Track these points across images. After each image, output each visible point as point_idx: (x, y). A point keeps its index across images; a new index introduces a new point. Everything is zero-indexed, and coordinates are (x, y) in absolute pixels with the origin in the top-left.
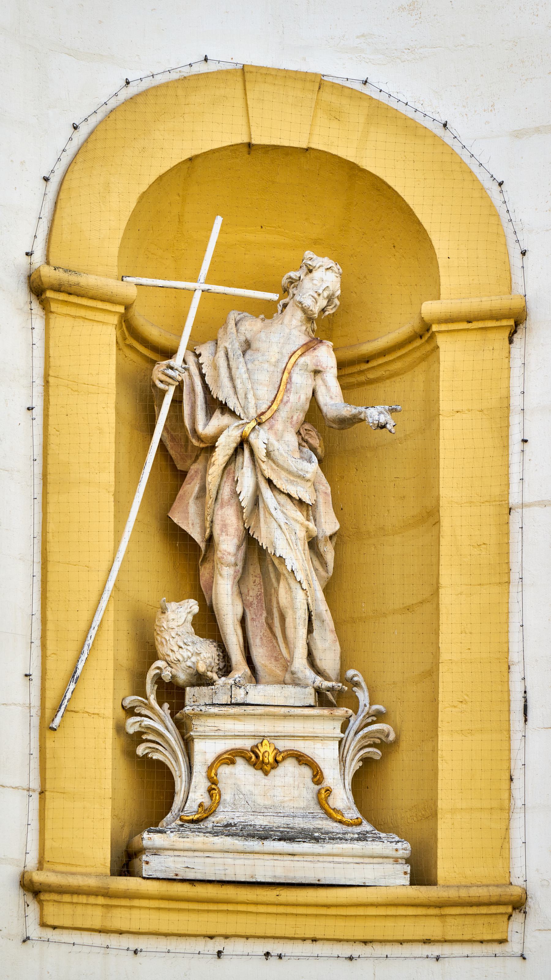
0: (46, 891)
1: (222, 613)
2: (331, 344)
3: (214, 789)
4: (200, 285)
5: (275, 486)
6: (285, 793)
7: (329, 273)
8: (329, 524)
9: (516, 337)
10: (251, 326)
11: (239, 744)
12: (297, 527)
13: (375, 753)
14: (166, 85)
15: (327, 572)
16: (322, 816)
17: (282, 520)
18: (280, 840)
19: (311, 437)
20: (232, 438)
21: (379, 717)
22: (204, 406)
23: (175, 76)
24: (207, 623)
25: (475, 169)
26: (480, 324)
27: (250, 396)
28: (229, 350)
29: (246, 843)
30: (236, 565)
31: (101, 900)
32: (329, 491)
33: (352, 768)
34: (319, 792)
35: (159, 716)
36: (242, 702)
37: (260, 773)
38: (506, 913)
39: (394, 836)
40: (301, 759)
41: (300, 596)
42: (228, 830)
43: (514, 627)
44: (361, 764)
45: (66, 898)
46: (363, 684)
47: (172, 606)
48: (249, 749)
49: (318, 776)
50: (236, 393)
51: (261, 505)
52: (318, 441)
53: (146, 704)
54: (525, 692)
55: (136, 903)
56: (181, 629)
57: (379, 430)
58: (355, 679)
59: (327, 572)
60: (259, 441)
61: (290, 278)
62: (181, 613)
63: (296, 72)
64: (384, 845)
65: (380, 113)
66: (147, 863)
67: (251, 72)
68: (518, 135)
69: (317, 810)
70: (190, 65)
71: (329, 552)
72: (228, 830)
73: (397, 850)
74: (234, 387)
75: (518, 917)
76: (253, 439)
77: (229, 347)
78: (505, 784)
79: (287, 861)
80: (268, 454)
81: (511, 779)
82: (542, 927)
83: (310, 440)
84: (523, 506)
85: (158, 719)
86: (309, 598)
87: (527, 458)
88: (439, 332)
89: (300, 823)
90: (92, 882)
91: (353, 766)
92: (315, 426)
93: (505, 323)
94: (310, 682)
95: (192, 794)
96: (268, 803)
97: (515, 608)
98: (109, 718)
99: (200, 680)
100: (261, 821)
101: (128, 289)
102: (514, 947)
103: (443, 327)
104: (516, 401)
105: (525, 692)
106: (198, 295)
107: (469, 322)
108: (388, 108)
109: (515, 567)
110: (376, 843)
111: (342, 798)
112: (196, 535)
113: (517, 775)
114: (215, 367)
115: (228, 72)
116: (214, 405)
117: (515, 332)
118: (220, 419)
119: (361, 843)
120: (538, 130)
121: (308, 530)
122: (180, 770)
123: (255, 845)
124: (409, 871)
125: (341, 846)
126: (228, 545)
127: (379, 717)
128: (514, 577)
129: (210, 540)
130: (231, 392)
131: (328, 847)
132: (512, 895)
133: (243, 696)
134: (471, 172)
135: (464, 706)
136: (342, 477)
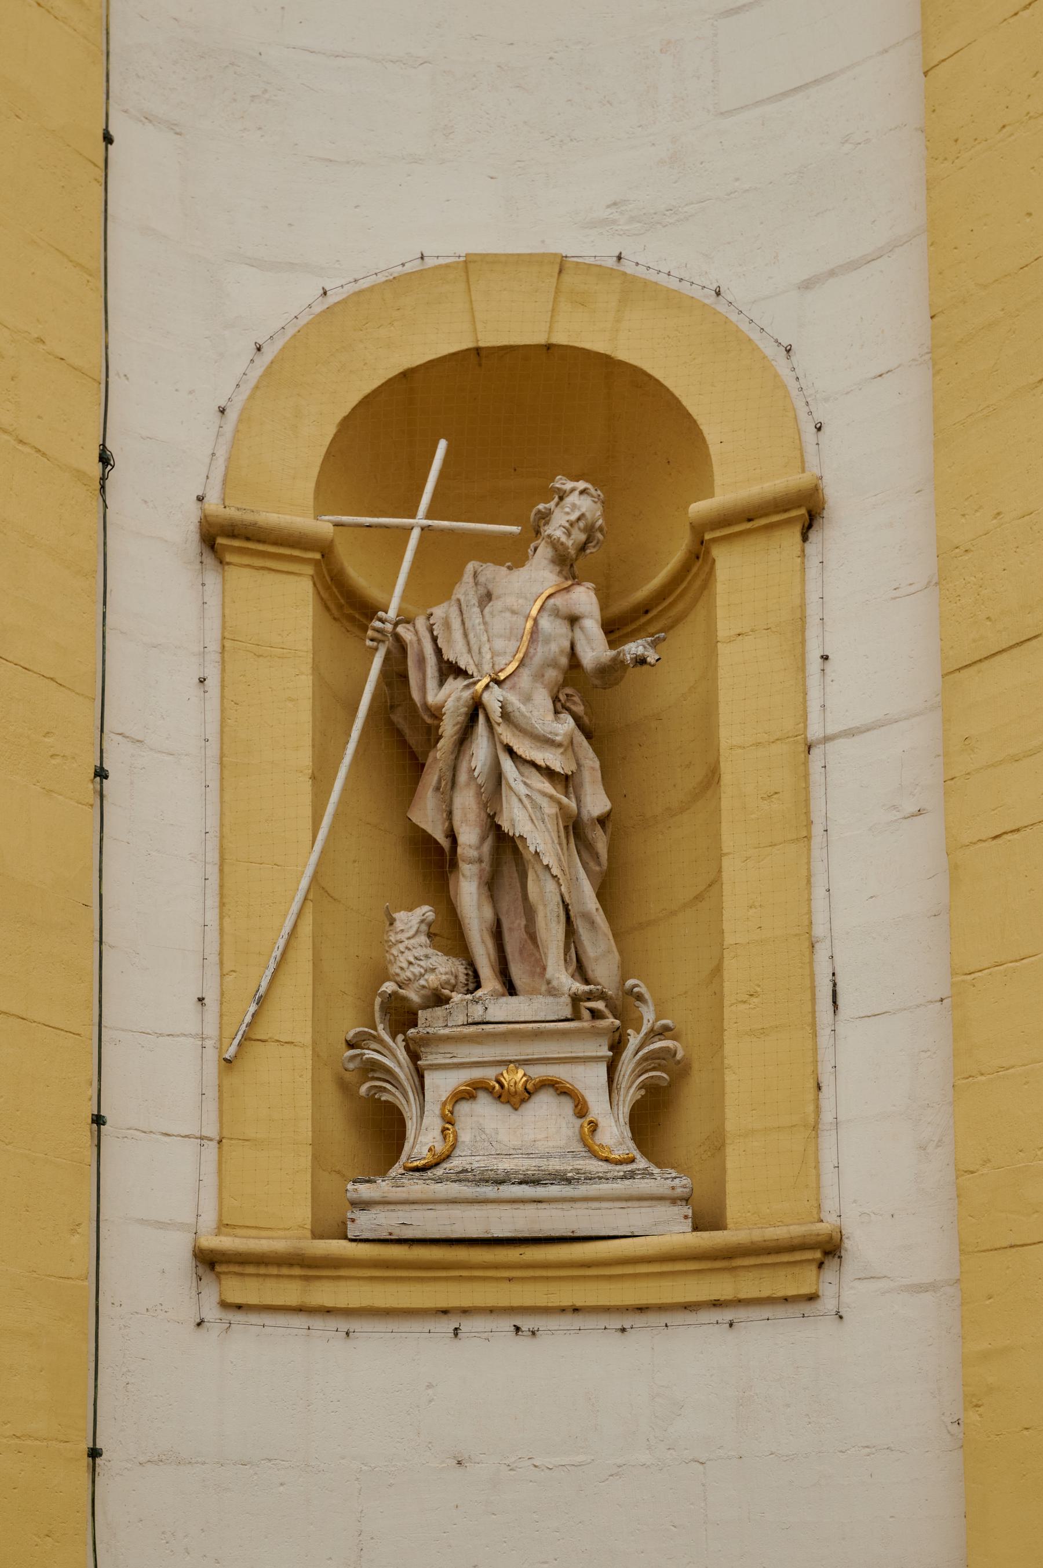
0: (221, 1262)
1: (467, 921)
2: (591, 585)
3: (448, 1129)
4: (420, 520)
5: (520, 757)
6: (541, 1132)
7: (584, 497)
8: (596, 802)
9: (813, 535)
10: (494, 574)
11: (477, 1074)
12: (544, 803)
13: (659, 1077)
14: (371, 289)
15: (599, 864)
16: (584, 1154)
17: (522, 790)
18: (520, 1183)
19: (575, 703)
20: (462, 702)
21: (663, 1032)
22: (436, 674)
23: (381, 278)
24: (449, 934)
25: (755, 336)
26: (763, 522)
27: (486, 649)
28: (462, 601)
29: (478, 1189)
30: (480, 861)
31: (297, 1271)
32: (597, 764)
33: (629, 1098)
34: (582, 1126)
35: (389, 1049)
36: (480, 1020)
37: (507, 1109)
38: (813, 1260)
39: (670, 1171)
40: (561, 1090)
41: (550, 886)
42: (462, 1176)
43: (819, 892)
44: (643, 1092)
45: (250, 1270)
46: (647, 996)
47: (401, 916)
48: (494, 1078)
49: (581, 1110)
50: (470, 651)
51: (503, 782)
52: (582, 708)
53: (374, 1037)
54: (834, 974)
55: (342, 1272)
56: (412, 941)
57: (639, 668)
58: (636, 990)
59: (599, 864)
60: (493, 699)
61: (539, 511)
62: (412, 919)
63: (530, 254)
64: (657, 1182)
65: (631, 288)
66: (353, 1220)
67: (475, 262)
68: (807, 285)
69: (579, 1147)
70: (403, 265)
71: (601, 842)
72: (462, 1176)
73: (673, 1188)
74: (468, 644)
75: (831, 1264)
76: (486, 697)
77: (462, 598)
78: (810, 1096)
79: (531, 1210)
80: (505, 715)
81: (819, 1088)
82: (862, 1275)
83: (574, 708)
84: (827, 739)
85: (394, 1057)
86: (563, 888)
87: (828, 679)
88: (714, 540)
89: (555, 1165)
90: (278, 1245)
91: (629, 1095)
92: (579, 691)
93: (794, 513)
94: (566, 989)
95: (423, 1139)
96: (517, 1143)
97: (818, 867)
98: (303, 1046)
99: (438, 999)
100: (505, 1165)
101: (323, 527)
102: (828, 1303)
103: (718, 534)
104: (813, 611)
105: (834, 974)
106: (415, 534)
107: (750, 520)
108: (646, 283)
109: (817, 817)
110: (646, 1181)
111: (614, 1133)
112: (440, 836)
113: (826, 1081)
114: (447, 625)
115: (447, 266)
116: (450, 670)
117: (810, 526)
118: (455, 686)
119: (627, 1182)
120: (832, 273)
121: (561, 806)
122: (411, 1110)
123: (489, 1191)
124: (690, 1215)
125: (601, 1186)
126: (469, 836)
127: (663, 1032)
128: (817, 830)
129: (452, 836)
130: (465, 650)
131: (583, 1190)
132: (818, 1235)
133: (481, 1013)
134: (750, 340)
135: (755, 1000)
136: (624, 758)
